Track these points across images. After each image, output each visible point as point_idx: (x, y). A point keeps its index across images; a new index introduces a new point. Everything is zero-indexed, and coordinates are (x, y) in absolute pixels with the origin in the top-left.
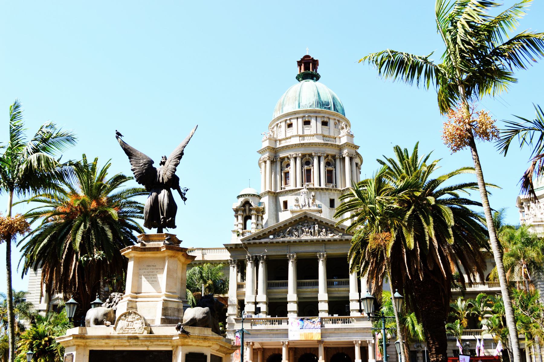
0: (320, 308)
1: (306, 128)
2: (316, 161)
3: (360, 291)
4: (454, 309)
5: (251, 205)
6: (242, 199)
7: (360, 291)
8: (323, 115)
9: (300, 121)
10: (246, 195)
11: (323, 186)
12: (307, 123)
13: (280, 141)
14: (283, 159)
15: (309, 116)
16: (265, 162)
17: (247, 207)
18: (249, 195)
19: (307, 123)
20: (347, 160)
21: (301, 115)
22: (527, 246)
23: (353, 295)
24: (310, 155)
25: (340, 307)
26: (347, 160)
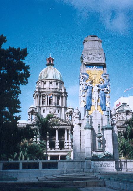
0: (49, 146)
1: (51, 85)
2: (46, 97)
3: (68, 140)
4: (49, 136)
5: (34, 111)
6: (32, 109)
7: (68, 140)
8: (40, 81)
9: (49, 82)
10: (32, 108)
11: (48, 105)
12: (51, 83)
13: (42, 89)
14: (43, 95)
15: (58, 82)
16: (37, 96)
17: (33, 112)
18: (33, 108)
19: (51, 83)
20: (64, 97)
21: (43, 81)
22: (36, 115)
23: (66, 141)
24: (45, 95)
25: (62, 145)
26: (64, 97)
